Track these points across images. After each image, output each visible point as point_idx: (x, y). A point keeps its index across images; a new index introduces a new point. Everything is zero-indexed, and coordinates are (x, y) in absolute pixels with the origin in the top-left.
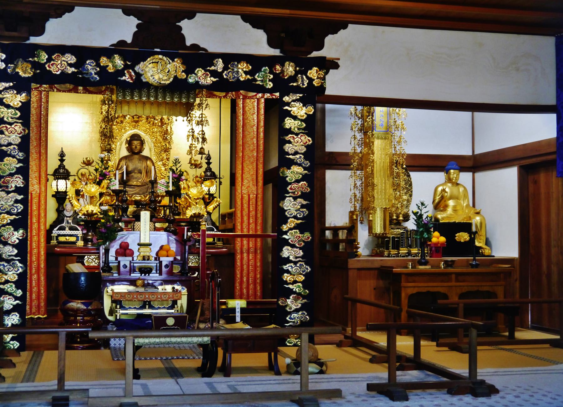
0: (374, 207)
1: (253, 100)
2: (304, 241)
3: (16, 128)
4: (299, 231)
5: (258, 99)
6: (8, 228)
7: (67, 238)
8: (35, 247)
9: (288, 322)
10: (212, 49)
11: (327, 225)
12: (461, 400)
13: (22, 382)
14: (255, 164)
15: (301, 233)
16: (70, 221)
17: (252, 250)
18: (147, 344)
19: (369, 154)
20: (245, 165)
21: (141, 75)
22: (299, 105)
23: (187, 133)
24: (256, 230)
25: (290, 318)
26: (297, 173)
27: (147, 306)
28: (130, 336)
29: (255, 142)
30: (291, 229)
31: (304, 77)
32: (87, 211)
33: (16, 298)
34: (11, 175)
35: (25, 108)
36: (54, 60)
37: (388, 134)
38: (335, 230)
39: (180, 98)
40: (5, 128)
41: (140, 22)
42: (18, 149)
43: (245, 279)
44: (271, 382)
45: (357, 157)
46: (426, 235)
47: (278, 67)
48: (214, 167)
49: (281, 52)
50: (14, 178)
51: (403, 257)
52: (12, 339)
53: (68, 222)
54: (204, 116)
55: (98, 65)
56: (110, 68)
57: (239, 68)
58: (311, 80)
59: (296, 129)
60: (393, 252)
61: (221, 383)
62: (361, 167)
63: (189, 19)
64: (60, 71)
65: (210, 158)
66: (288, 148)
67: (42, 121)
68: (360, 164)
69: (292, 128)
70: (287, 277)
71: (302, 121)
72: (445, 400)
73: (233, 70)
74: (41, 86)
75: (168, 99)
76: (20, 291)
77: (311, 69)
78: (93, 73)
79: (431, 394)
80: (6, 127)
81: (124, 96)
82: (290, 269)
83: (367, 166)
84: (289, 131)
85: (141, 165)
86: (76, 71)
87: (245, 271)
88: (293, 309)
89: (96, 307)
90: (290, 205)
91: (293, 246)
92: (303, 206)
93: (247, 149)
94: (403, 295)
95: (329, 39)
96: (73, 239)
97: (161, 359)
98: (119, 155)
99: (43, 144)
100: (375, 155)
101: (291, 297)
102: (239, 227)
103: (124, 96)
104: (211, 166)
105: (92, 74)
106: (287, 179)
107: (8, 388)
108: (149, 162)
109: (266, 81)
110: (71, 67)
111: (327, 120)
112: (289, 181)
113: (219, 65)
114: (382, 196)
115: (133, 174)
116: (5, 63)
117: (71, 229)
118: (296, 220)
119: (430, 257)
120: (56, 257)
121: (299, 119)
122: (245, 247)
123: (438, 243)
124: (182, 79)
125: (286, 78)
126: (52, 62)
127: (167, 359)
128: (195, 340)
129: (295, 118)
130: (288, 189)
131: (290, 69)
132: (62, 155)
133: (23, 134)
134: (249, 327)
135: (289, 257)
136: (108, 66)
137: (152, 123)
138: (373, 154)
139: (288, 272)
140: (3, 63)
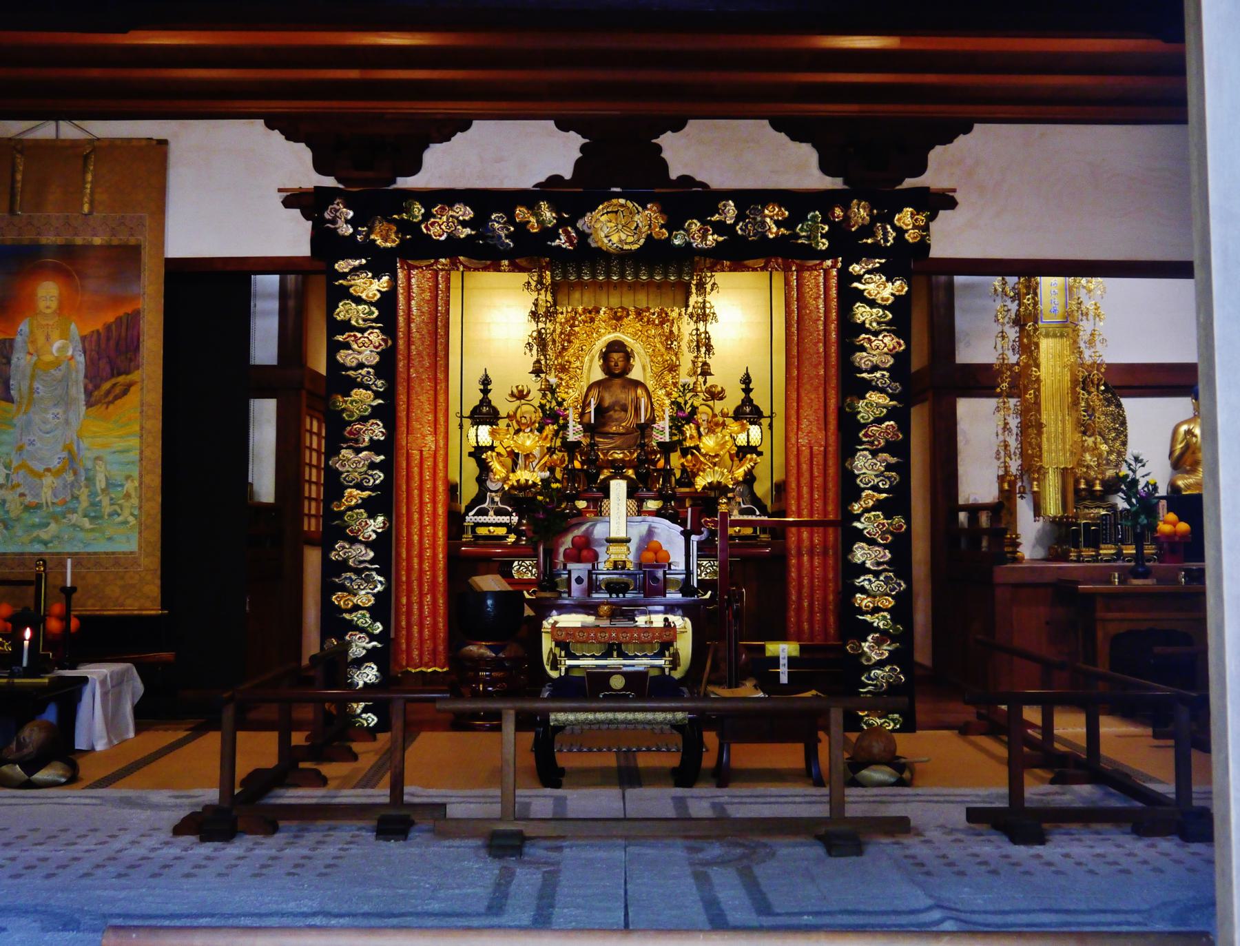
0: (1041, 467)
5: (825, 271)
10: (717, 181)
11: (961, 501)
12: (1153, 846)
13: (354, 787)
14: (821, 390)
16: (497, 499)
18: (572, 724)
19: (1030, 366)
20: (803, 393)
21: (589, 235)
22: (880, 278)
23: (526, 339)
24: (826, 513)
25: (869, 678)
27: (615, 654)
30: (867, 510)
32: (518, 481)
33: (372, 637)
35: (387, 303)
36: (434, 216)
37: (1068, 326)
38: (974, 510)
42: (375, 374)
44: (797, 799)
46: (1143, 520)
47: (838, 212)
49: (845, 183)
51: (1107, 561)
52: (365, 710)
53: (493, 501)
54: (708, 305)
55: (511, 220)
58: (900, 232)
59: (874, 324)
60: (1088, 552)
63: (674, 131)
66: (862, 359)
68: (1012, 386)
70: (862, 600)
71: (884, 308)
72: (1118, 846)
73: (754, 219)
74: (436, 262)
76: (378, 624)
77: (900, 211)
79: (1098, 833)
81: (565, 275)
82: (866, 584)
83: (1026, 389)
85: (626, 397)
87: (805, 591)
90: (866, 466)
91: (872, 542)
92: (889, 467)
93: (807, 363)
94: (1100, 634)
95: (937, 155)
96: (502, 531)
98: (588, 379)
101: (870, 638)
104: (752, 395)
105: (500, 237)
107: (323, 797)
110: (464, 227)
111: (958, 304)
114: (1058, 445)
117: (498, 512)
119: (1161, 562)
120: (464, 560)
121: (880, 306)
122: (806, 543)
123: (1175, 534)
124: (660, 240)
127: (629, 750)
128: (660, 716)
129: (872, 303)
131: (861, 213)
132: (486, 382)
133: (384, 347)
134: (761, 695)
135: (864, 563)
138: (1038, 366)
139: (863, 590)
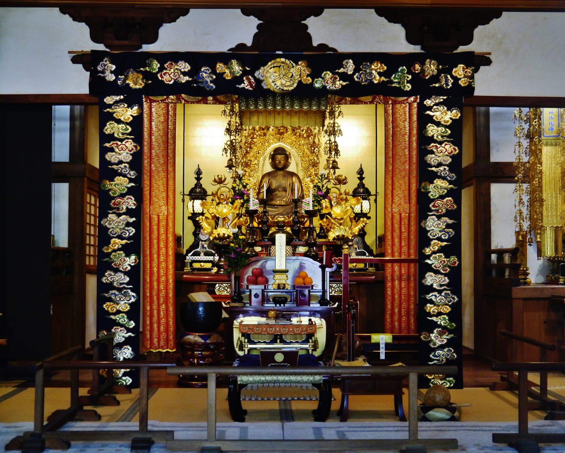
0: (542, 226)
1: (404, 105)
2: (449, 267)
3: (127, 144)
4: (444, 255)
5: (410, 104)
6: (119, 254)
7: (202, 264)
8: (162, 274)
9: (432, 360)
10: (342, 49)
11: (493, 247)
15: (446, 257)
16: (206, 246)
17: (404, 277)
18: (251, 383)
21: (262, 81)
25: (435, 356)
26: (441, 188)
27: (278, 341)
28: (213, 373)
29: (407, 153)
30: (434, 253)
31: (449, 76)
32: (218, 234)
33: (128, 330)
34: (122, 196)
35: (137, 124)
36: (166, 69)
38: (501, 253)
39: (310, 106)
40: (115, 145)
41: (261, 22)
42: (130, 167)
43: (396, 310)
45: (523, 168)
47: (417, 67)
48: (369, 183)
49: (422, 49)
50: (125, 199)
52: (125, 374)
54: (336, 125)
55: (214, 72)
56: (227, 75)
57: (372, 70)
58: (456, 79)
59: (440, 137)
61: (331, 429)
62: (527, 178)
64: (173, 81)
65: (363, 173)
66: (431, 159)
67: (169, 136)
69: (435, 136)
70: (430, 308)
71: (446, 127)
73: (365, 71)
74: (168, 98)
75: (297, 108)
76: (132, 322)
77: (456, 66)
78: (209, 81)
80: (117, 144)
81: (247, 106)
82: (433, 298)
84: (432, 140)
86: (190, 79)
87: (397, 302)
88: (437, 345)
89: (215, 341)
91: (437, 272)
93: (398, 162)
95: (479, 31)
96: (209, 265)
97: (280, 399)
98: (262, 171)
99: (171, 161)
100: (544, 164)
101: (435, 331)
102: (390, 251)
103: (247, 106)
104: (364, 181)
105: (207, 82)
106: (430, 195)
107: (98, 427)
108: (294, 179)
109: (403, 83)
110: (184, 75)
112: (432, 197)
113: (350, 67)
115: (277, 192)
116: (115, 75)
117: (206, 254)
118: (439, 242)
121: (443, 126)
122: (397, 273)
124: (307, 84)
125: (427, 78)
126: (165, 71)
127: (287, 400)
129: (438, 124)
130: (431, 206)
131: (431, 68)
132: (199, 173)
133: (135, 150)
134: (368, 365)
135: (432, 285)
136: (225, 73)
137: (298, 134)
138: (541, 163)
139: (431, 302)
140: (113, 75)
